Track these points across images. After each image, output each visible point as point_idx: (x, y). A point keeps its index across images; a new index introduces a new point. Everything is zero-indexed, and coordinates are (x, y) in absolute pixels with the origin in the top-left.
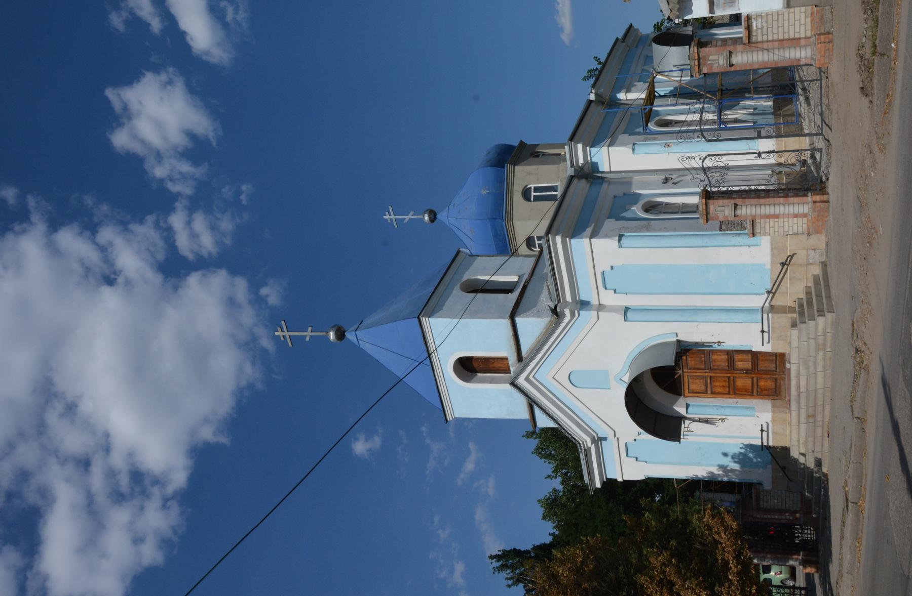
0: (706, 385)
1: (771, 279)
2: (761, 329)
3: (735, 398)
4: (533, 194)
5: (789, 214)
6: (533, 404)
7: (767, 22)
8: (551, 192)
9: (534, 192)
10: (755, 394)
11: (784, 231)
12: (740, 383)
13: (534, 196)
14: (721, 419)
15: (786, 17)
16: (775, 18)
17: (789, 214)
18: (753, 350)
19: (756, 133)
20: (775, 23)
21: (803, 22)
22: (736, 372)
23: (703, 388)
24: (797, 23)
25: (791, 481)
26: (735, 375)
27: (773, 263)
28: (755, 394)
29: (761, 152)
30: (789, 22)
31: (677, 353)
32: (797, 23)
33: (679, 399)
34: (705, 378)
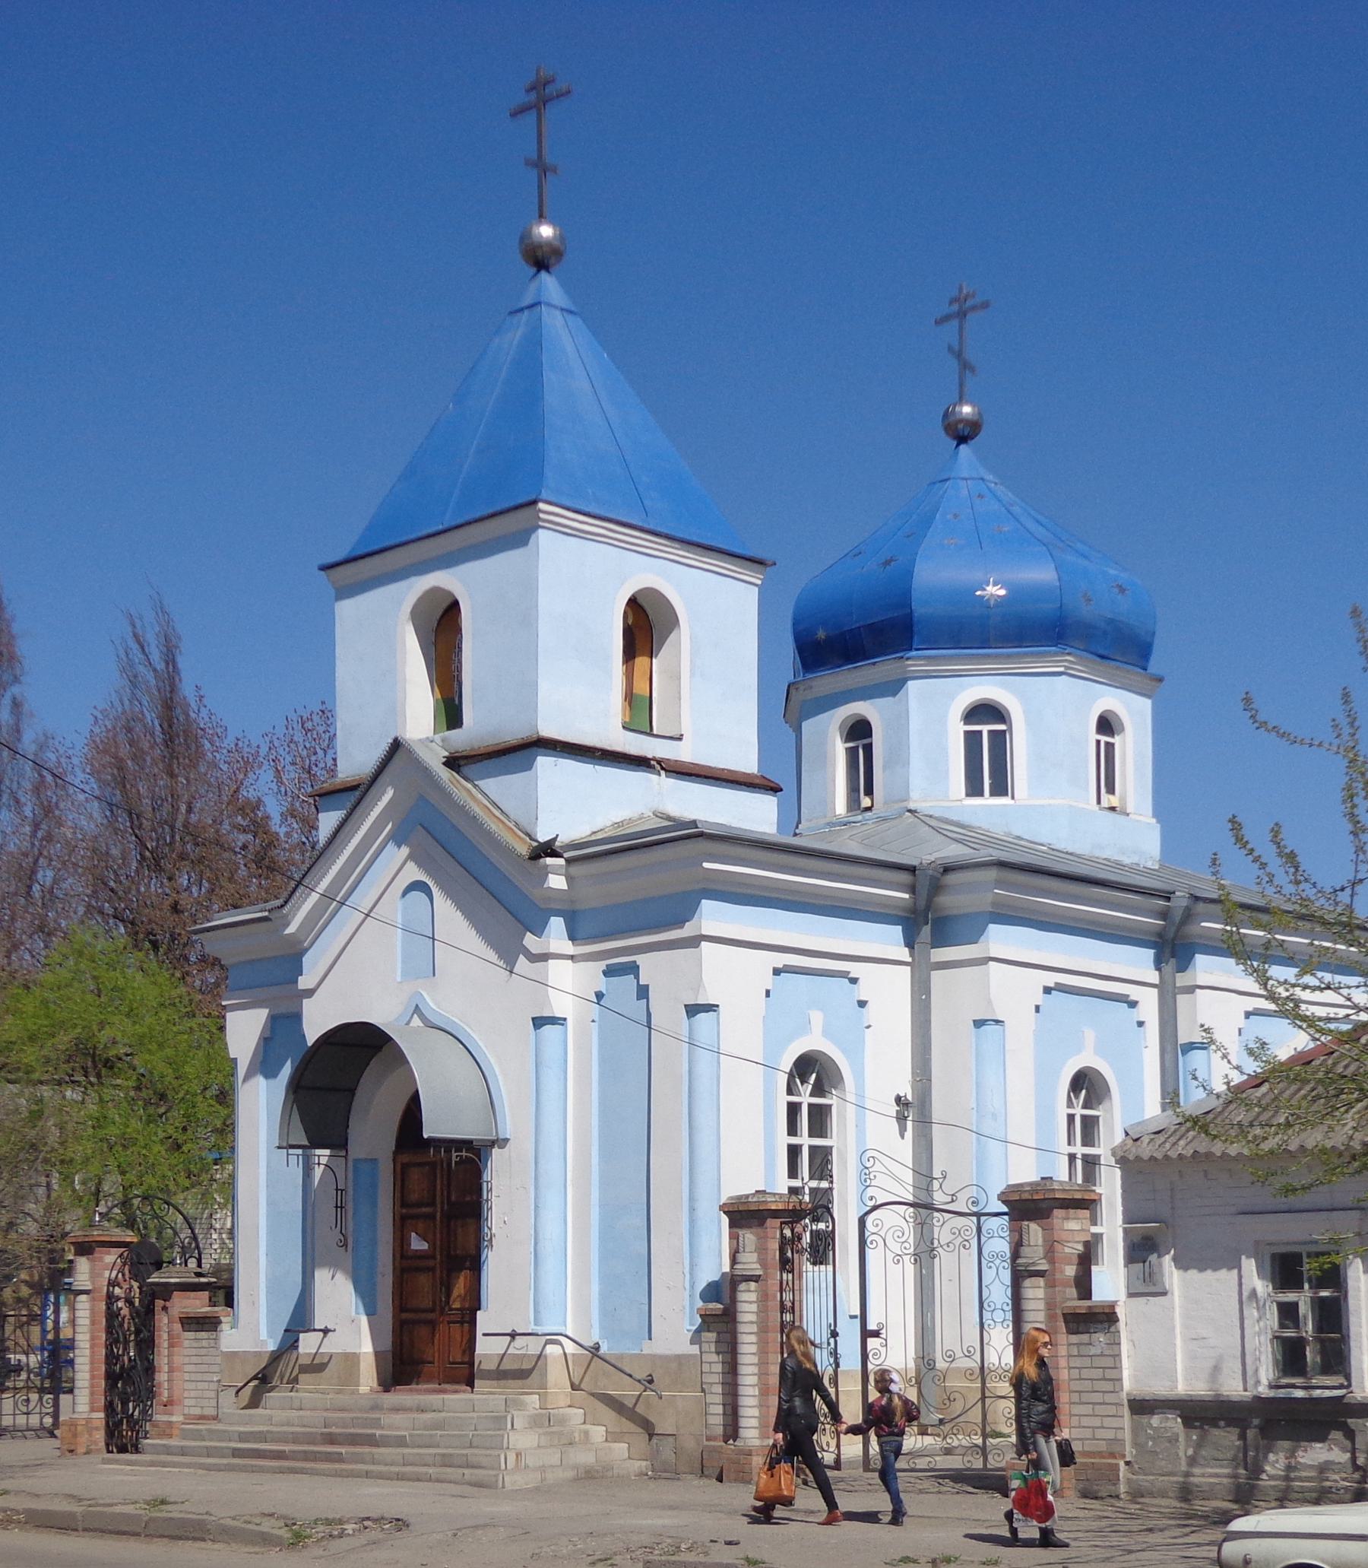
0: (419, 1205)
1: (621, 1357)
2: (519, 1331)
3: (394, 1269)
4: (985, 729)
5: (1057, 1356)
6: (357, 793)
7: (1102, 1355)
8: (991, 777)
9: (990, 732)
10: (404, 1316)
11: (712, 1384)
12: (424, 1281)
13: (980, 732)
14: (346, 1240)
15: (1109, 1398)
16: (1109, 1374)
17: (1057, 1356)
18: (478, 1312)
19: (875, 1328)
20: (1097, 1373)
21: (1100, 1433)
22: (445, 1272)
23: (414, 1197)
24: (1097, 1422)
25: (237, 1392)
26: (438, 1272)
27: (654, 1358)
28: (404, 1316)
29: (837, 1338)
30: (1100, 1404)
31: (470, 1142)
32: (1097, 1422)
33: (1195, 975)
34: (433, 1204)
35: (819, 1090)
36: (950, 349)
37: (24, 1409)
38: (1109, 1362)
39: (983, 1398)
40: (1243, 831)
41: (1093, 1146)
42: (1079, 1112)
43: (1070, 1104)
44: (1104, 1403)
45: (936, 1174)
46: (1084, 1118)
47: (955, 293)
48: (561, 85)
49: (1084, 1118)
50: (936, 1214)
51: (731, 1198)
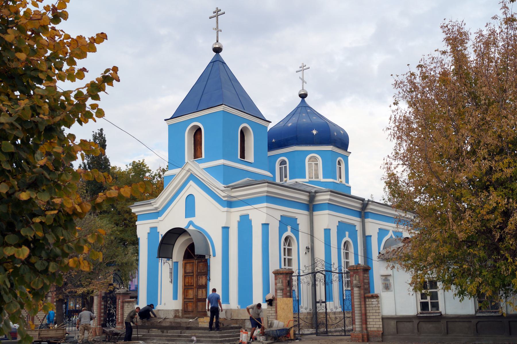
7: (375, 307)
10: (185, 300)
19: (318, 301)
21: (375, 326)
23: (188, 271)
28: (185, 300)
32: (374, 323)
35: (289, 245)
36: (300, 78)
37: (74, 325)
38: (377, 308)
39: (344, 318)
40: (108, 87)
41: (290, 256)
42: (287, 247)
43: (284, 245)
44: (376, 319)
45: (332, 264)
46: (288, 249)
47: (301, 65)
48: (387, 131)
49: (288, 249)
50: (332, 273)
51: (275, 270)
